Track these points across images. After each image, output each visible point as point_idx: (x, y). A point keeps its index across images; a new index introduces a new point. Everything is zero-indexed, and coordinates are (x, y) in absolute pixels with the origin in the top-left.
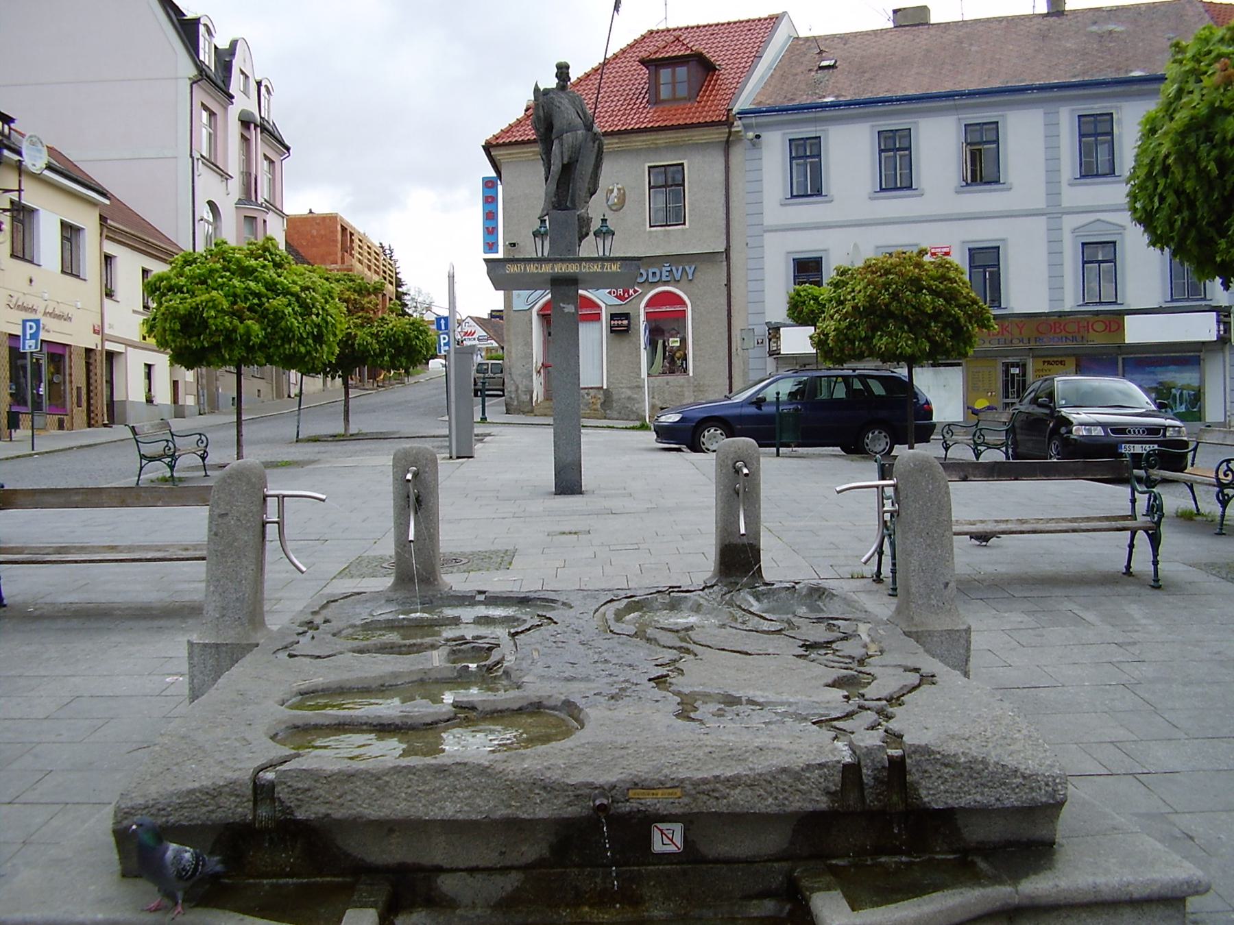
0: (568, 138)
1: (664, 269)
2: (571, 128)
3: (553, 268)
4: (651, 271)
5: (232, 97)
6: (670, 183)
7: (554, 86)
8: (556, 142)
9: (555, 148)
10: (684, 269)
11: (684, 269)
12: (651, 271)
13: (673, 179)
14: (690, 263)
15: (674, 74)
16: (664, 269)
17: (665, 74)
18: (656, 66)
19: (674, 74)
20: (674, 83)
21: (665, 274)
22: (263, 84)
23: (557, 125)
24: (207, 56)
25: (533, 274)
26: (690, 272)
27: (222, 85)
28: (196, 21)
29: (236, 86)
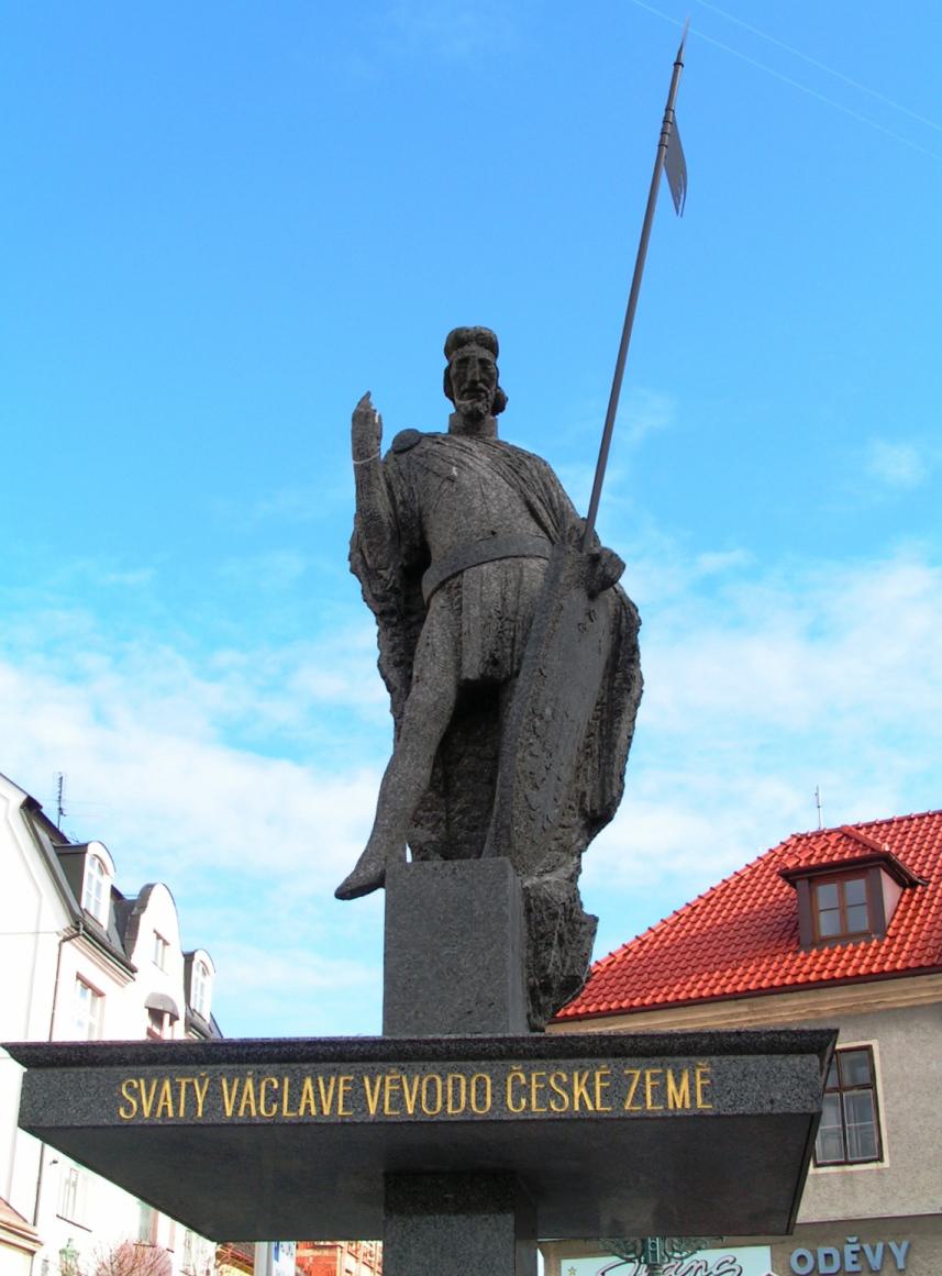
0: (486, 585)
1: (848, 1249)
2: (493, 546)
3: (355, 1098)
4: (822, 1251)
5: (133, 970)
6: (847, 1081)
7: (442, 427)
8: (438, 602)
9: (435, 631)
10: (887, 1249)
11: (887, 1249)
12: (822, 1251)
13: (854, 1078)
14: (898, 1235)
15: (842, 892)
16: (848, 1249)
17: (826, 893)
18: (811, 880)
19: (842, 892)
20: (843, 909)
21: (849, 1257)
22: (198, 957)
23: (441, 539)
24: (101, 911)
25: (251, 1126)
26: (899, 1254)
27: (123, 957)
28: (81, 850)
29: (142, 953)
